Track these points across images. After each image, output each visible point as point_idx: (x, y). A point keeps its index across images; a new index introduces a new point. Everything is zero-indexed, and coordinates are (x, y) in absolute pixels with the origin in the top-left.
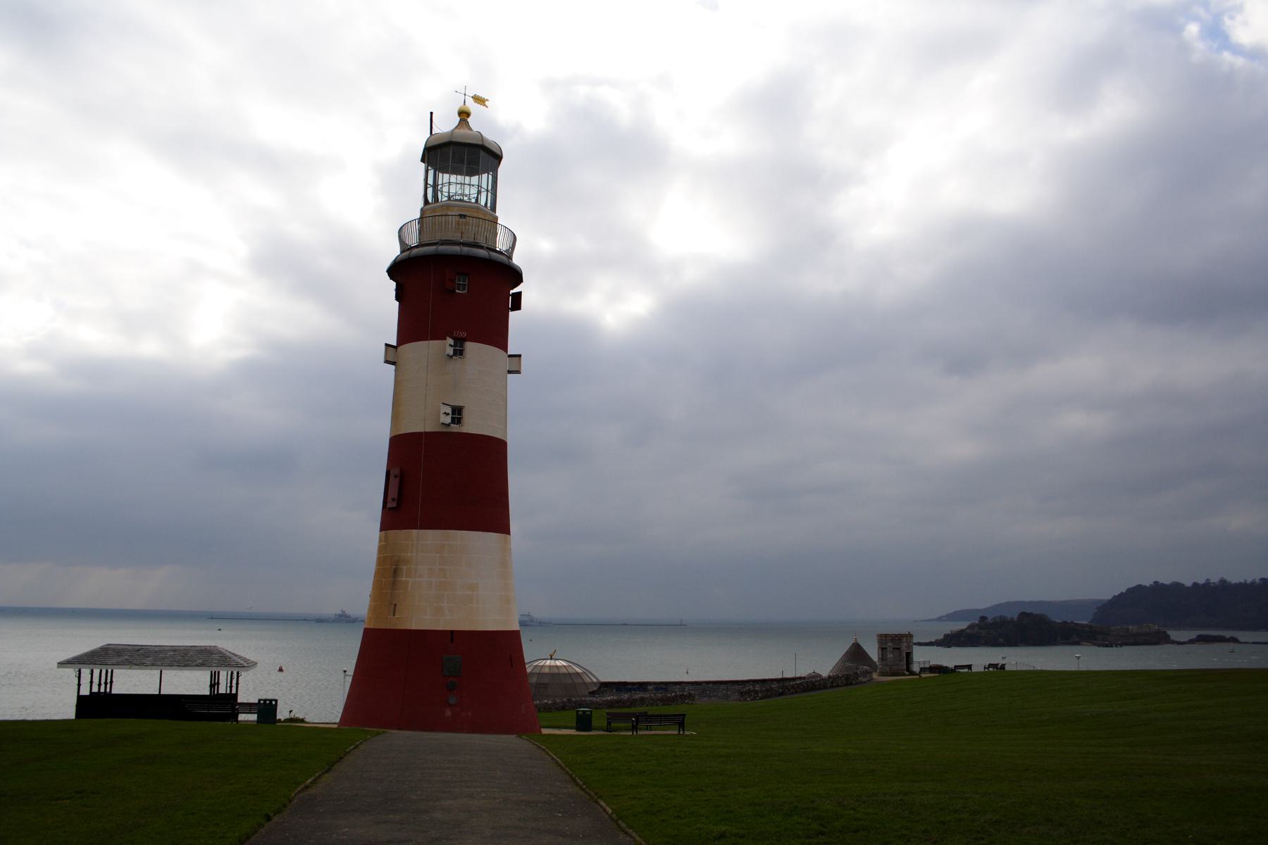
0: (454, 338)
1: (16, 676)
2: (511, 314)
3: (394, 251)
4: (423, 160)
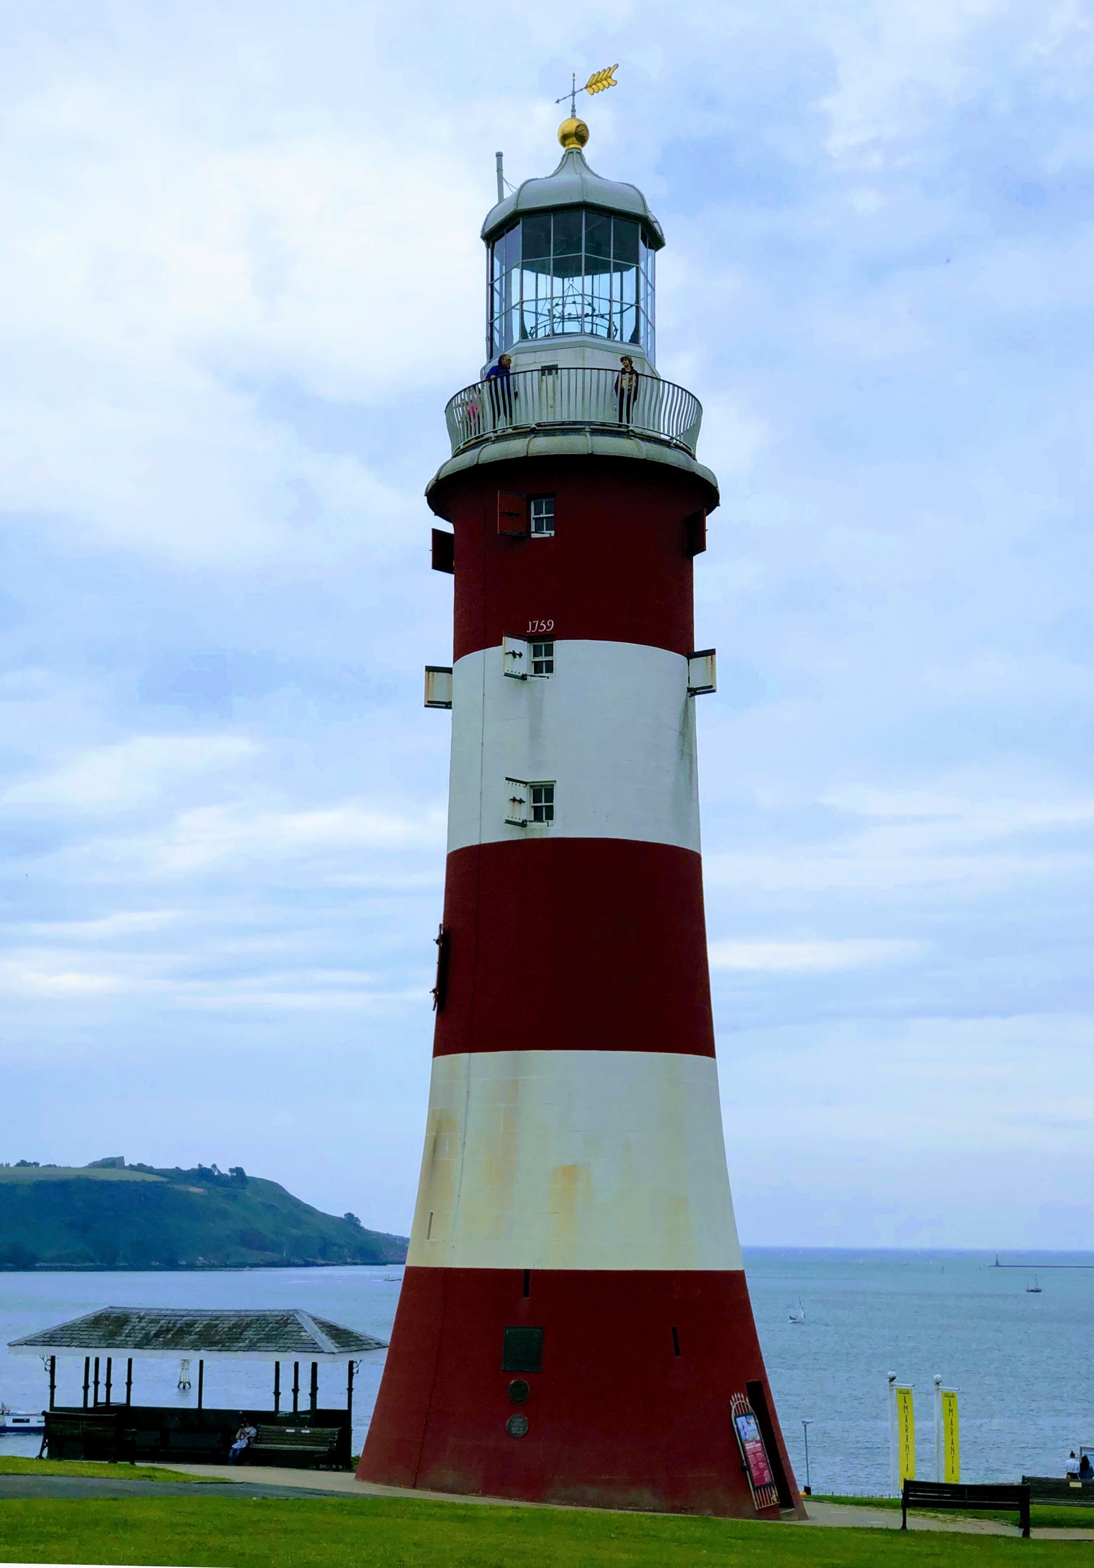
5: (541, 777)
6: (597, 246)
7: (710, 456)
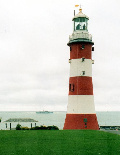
1: (1, 127)
3: (68, 42)
5: (83, 71)
6: (80, 20)
7: (93, 41)
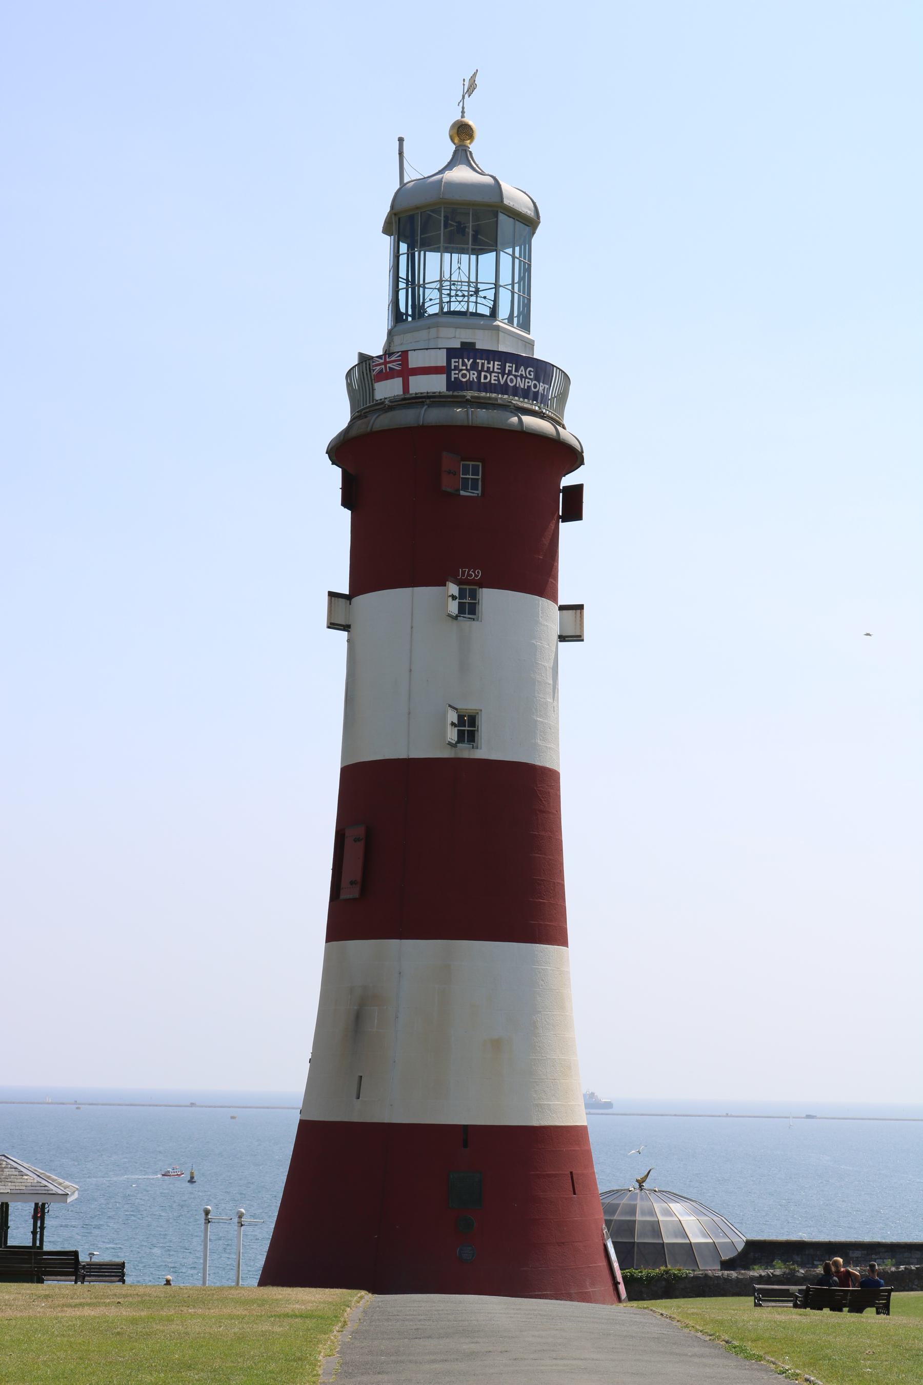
0: (459, 583)
2: (565, 528)
4: (387, 230)
5: (469, 706)
